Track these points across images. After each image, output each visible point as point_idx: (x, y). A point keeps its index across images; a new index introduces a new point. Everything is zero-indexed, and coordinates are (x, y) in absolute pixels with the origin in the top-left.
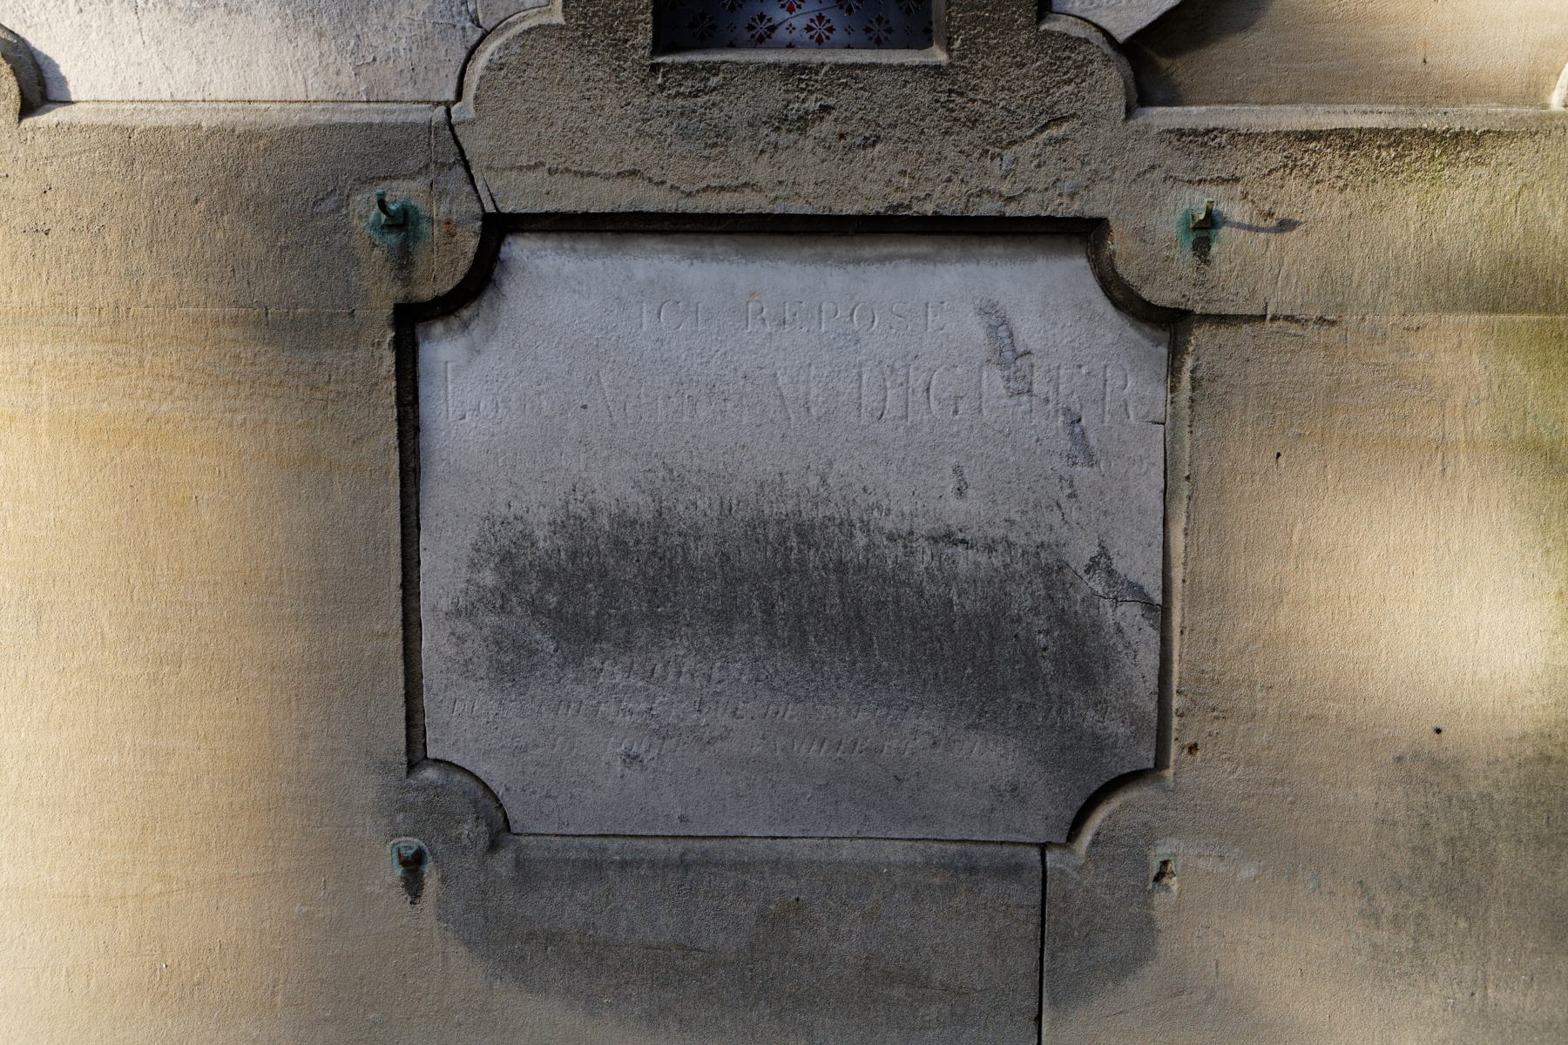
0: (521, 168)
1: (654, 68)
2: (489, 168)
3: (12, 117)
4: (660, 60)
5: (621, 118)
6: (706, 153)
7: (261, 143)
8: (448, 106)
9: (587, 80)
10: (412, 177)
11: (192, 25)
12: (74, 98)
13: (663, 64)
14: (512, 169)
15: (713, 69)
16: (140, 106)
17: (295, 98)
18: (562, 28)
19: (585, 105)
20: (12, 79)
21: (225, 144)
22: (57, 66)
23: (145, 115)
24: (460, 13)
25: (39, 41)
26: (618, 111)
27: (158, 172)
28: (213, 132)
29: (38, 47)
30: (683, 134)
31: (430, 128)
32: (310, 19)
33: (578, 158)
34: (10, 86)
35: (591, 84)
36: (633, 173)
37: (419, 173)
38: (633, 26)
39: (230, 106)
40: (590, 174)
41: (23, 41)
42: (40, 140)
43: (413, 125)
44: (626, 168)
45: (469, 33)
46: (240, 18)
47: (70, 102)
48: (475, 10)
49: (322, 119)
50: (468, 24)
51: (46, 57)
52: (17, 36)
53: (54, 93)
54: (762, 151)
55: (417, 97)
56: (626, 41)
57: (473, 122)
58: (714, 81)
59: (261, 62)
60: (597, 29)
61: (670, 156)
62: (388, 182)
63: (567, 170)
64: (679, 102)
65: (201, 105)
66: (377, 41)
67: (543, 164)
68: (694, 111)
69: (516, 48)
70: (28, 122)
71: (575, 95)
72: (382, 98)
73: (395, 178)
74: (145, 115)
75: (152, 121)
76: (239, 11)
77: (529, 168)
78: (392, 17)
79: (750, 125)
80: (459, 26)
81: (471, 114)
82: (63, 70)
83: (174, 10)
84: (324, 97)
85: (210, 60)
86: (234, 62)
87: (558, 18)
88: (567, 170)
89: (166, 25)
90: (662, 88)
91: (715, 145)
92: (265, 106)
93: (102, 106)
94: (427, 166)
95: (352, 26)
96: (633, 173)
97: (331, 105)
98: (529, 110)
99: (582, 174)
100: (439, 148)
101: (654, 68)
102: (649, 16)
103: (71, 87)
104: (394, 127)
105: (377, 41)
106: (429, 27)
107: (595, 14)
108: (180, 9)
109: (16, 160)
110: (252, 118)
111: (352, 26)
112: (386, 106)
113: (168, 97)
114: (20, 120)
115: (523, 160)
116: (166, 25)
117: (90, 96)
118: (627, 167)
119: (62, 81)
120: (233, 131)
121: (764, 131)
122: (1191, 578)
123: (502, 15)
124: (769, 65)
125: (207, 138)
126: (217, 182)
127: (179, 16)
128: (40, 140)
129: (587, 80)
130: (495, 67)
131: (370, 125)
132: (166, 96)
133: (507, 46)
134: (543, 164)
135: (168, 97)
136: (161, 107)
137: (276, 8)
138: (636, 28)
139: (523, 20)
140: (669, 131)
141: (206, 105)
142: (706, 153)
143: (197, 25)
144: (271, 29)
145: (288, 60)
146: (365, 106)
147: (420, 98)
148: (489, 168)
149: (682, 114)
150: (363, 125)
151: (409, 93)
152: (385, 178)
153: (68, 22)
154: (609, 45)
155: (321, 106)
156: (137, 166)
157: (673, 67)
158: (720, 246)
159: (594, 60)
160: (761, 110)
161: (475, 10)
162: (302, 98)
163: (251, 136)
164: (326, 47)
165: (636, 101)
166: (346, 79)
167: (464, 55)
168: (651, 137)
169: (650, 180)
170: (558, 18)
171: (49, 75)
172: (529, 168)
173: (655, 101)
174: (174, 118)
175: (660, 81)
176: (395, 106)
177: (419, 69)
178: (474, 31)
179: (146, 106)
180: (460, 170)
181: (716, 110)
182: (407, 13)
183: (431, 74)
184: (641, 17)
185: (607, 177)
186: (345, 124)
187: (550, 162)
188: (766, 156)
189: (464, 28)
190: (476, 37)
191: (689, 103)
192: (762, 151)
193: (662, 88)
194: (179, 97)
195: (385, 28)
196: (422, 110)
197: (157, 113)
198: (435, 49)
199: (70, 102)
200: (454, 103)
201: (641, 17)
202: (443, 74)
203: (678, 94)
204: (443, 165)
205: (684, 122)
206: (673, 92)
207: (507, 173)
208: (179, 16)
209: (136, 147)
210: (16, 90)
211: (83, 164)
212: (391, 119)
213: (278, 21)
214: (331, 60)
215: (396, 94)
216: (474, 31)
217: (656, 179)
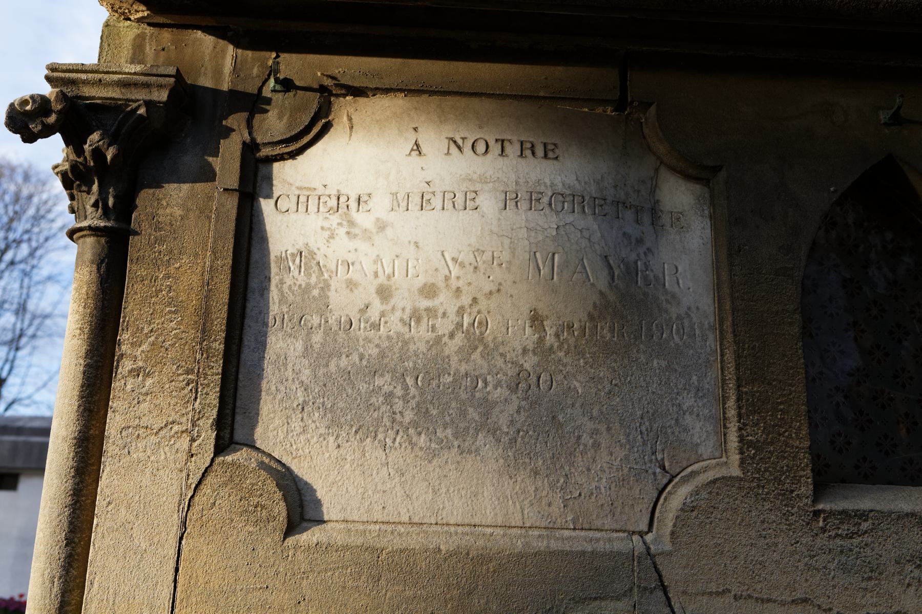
0: (711, 594)
1: (817, 513)
2: (684, 593)
3: (278, 536)
4: (820, 506)
5: (792, 554)
6: (864, 585)
7: (491, 566)
8: (641, 534)
9: (763, 522)
10: (618, 599)
11: (430, 462)
12: (326, 518)
13: (823, 511)
14: (703, 594)
15: (863, 515)
16: (384, 527)
17: (513, 524)
18: (741, 479)
19: (762, 542)
20: (282, 504)
21: (460, 565)
22: (315, 491)
23: (390, 537)
24: (651, 461)
25: (301, 469)
26: (790, 548)
27: (401, 588)
28: (451, 554)
29: (300, 475)
30: (844, 568)
31: (631, 556)
32: (527, 460)
33: (758, 587)
34: (280, 510)
35: (766, 525)
36: (805, 600)
37: (625, 595)
38: (797, 480)
39: (460, 529)
40: (769, 600)
41: (288, 469)
42: (300, 556)
43: (619, 553)
44: (799, 596)
45: (659, 477)
46: (470, 458)
47: (325, 522)
48: (663, 459)
49: (542, 545)
50: (658, 470)
51: (306, 483)
52: (283, 465)
53: (310, 514)
54: (909, 585)
55: (615, 526)
56: (792, 491)
57: (670, 554)
58: (865, 526)
59: (486, 494)
60: (768, 481)
61: (834, 587)
62: (597, 603)
63: (750, 596)
64: (839, 542)
65: (434, 528)
66: (582, 480)
67: (729, 591)
68: (851, 550)
69: (704, 495)
70: (291, 541)
71: (753, 534)
72: (586, 526)
73: (602, 599)
74: (390, 537)
75: (398, 543)
76: (470, 452)
77: (718, 594)
78: (594, 460)
79: (897, 562)
80: (650, 471)
81: (668, 547)
82: (319, 495)
83: (416, 449)
84: (538, 524)
85: (444, 490)
86: (463, 493)
87: (736, 472)
88: (750, 596)
89: (409, 461)
90: (823, 530)
91: (870, 579)
92: (489, 530)
93: (351, 526)
94: (631, 589)
95: (562, 467)
96: (805, 600)
97: (544, 532)
98: (717, 545)
99: (762, 600)
100: (642, 575)
101: (817, 513)
102: (809, 472)
103: (325, 510)
104: (604, 555)
105: (582, 480)
106: (626, 470)
107: (766, 470)
108: (421, 448)
109: (277, 573)
110: (480, 543)
111: (562, 467)
112: (591, 534)
113: (407, 520)
114: (285, 539)
115: (713, 587)
116: (409, 461)
117: (340, 517)
118: (799, 595)
119: (318, 503)
120: (468, 554)
121: (909, 567)
122: (188, 487)
123: (685, 464)
124: (907, 515)
125: (445, 560)
126: (451, 599)
127: (420, 454)
128: (300, 556)
129: (763, 522)
130: (687, 509)
131: (583, 553)
132: (405, 518)
133: (697, 492)
134: (729, 591)
135: (407, 520)
136: (402, 529)
137: (500, 451)
138: (799, 481)
139: (706, 469)
140: (832, 566)
141: (439, 528)
142: (864, 585)
143: (434, 462)
144: (495, 467)
145: (508, 492)
146: (573, 534)
147: (618, 527)
148: (684, 593)
149: (842, 552)
150: (577, 552)
151: (608, 523)
152: (595, 599)
153: (327, 455)
154: (779, 494)
155: (536, 533)
156: (383, 582)
157: (831, 513)
158: (247, 355)
159: (767, 505)
160: (904, 551)
161: (663, 459)
162: (519, 524)
163: (483, 559)
164: (540, 484)
165: (804, 541)
166: (555, 510)
167: (655, 495)
168: (818, 570)
169: (819, 607)
170: (736, 472)
171: (307, 498)
172: (718, 594)
173: (818, 540)
174: (415, 541)
175: (821, 524)
176: (598, 535)
177: (618, 504)
178: (663, 476)
179: (389, 528)
180: (660, 594)
181: (868, 550)
182: (607, 458)
183: (627, 509)
184: (802, 473)
185: (783, 604)
186: (562, 551)
187: (735, 590)
188: (912, 590)
189: (654, 473)
190: (665, 481)
191: (846, 543)
192: (909, 585)
193: (823, 530)
194: (416, 520)
195: (589, 470)
196: (622, 539)
197: (400, 535)
198: (631, 488)
199: (325, 522)
200: (647, 533)
201: (802, 473)
202: (637, 509)
203: (837, 535)
204: (645, 589)
205: (844, 559)
206: (833, 533)
207: (699, 598)
208: (420, 454)
209: (383, 566)
210: (284, 514)
211: (336, 579)
212: (600, 547)
213: (501, 461)
214: (544, 493)
215: (598, 523)
216: (663, 476)
217: (824, 607)
